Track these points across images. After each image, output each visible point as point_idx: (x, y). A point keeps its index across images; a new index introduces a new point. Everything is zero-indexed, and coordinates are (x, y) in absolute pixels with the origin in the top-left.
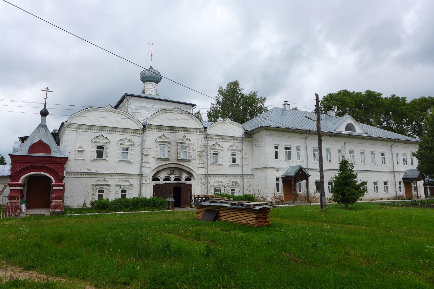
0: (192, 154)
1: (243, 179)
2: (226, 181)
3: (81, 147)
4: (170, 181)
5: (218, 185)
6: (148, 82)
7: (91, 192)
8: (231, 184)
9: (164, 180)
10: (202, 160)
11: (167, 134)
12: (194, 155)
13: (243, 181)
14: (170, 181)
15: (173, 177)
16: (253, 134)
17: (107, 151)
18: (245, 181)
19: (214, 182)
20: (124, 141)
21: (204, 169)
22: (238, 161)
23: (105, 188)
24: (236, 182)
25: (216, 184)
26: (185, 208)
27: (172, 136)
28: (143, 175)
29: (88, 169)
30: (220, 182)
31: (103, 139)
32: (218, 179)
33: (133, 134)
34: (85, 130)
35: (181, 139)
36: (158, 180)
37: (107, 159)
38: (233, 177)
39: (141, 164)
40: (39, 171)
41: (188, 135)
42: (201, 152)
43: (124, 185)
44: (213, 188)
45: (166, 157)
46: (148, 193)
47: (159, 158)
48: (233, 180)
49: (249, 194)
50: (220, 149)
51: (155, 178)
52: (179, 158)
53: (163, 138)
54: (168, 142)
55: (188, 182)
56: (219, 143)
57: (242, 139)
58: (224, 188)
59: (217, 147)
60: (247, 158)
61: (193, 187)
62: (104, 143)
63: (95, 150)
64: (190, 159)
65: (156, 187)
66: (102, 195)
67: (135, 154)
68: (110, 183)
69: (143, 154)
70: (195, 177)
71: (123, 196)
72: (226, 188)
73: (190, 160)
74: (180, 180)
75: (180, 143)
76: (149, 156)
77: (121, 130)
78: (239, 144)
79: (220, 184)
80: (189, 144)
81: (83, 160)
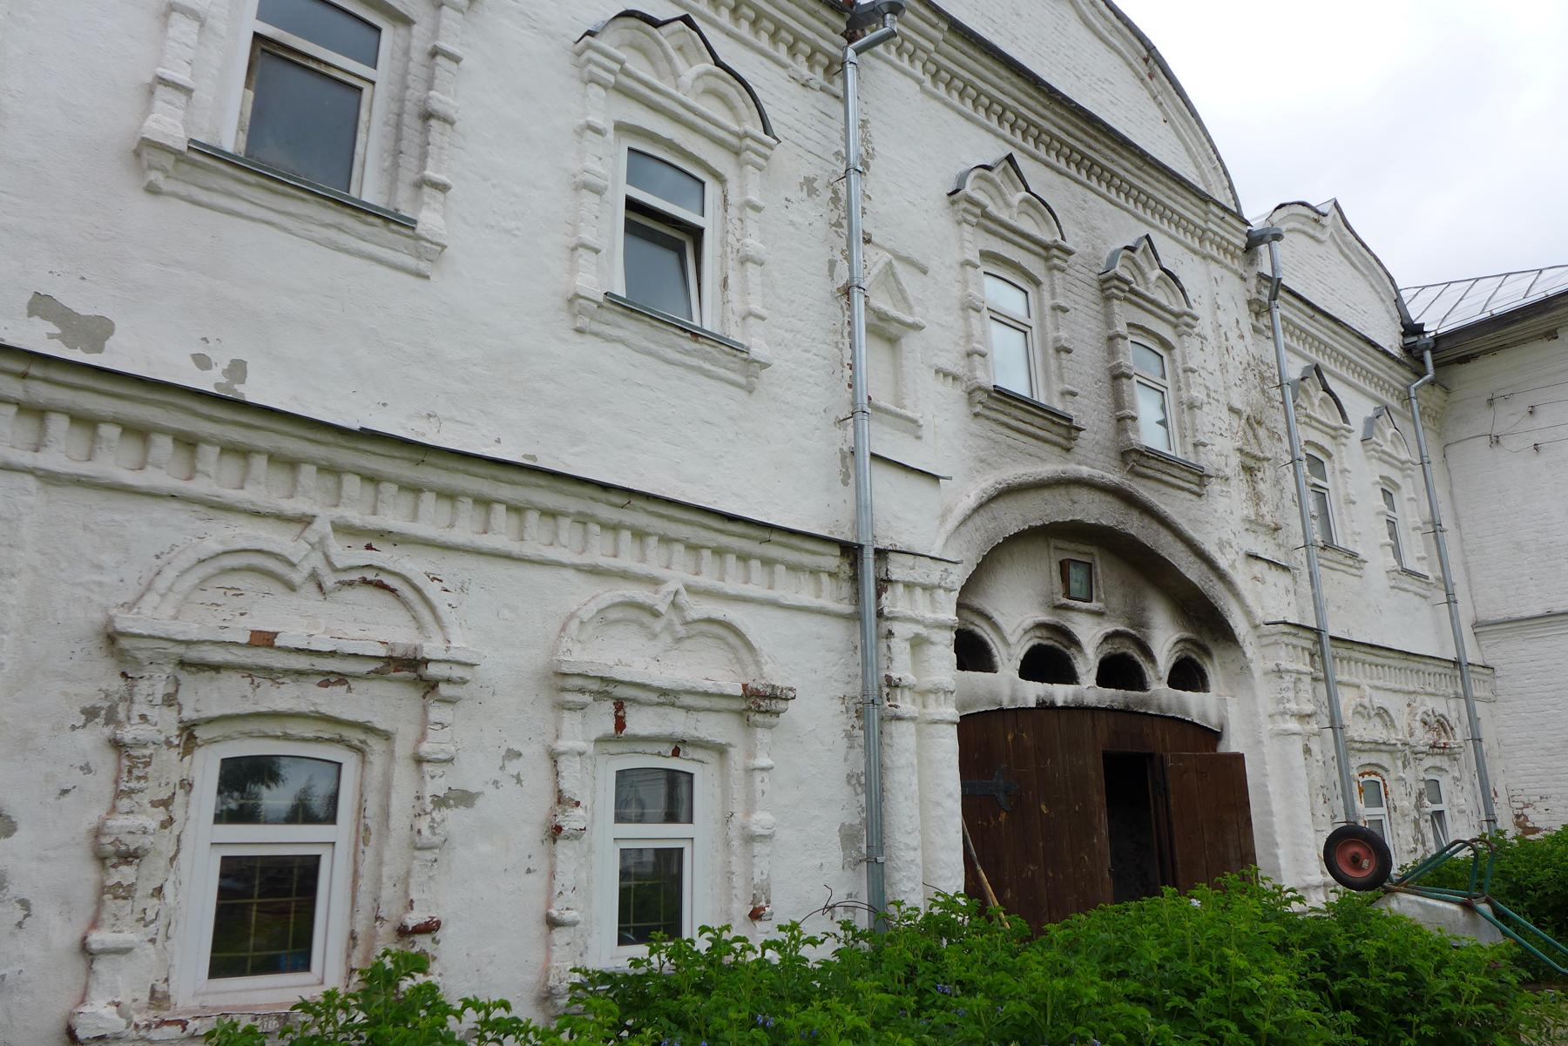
16: (1465, 359)
24: (1442, 725)
28: (898, 569)
30: (1382, 713)
37: (430, 219)
43: (667, 697)
66: (669, 862)
68: (462, 643)
70: (1250, 650)
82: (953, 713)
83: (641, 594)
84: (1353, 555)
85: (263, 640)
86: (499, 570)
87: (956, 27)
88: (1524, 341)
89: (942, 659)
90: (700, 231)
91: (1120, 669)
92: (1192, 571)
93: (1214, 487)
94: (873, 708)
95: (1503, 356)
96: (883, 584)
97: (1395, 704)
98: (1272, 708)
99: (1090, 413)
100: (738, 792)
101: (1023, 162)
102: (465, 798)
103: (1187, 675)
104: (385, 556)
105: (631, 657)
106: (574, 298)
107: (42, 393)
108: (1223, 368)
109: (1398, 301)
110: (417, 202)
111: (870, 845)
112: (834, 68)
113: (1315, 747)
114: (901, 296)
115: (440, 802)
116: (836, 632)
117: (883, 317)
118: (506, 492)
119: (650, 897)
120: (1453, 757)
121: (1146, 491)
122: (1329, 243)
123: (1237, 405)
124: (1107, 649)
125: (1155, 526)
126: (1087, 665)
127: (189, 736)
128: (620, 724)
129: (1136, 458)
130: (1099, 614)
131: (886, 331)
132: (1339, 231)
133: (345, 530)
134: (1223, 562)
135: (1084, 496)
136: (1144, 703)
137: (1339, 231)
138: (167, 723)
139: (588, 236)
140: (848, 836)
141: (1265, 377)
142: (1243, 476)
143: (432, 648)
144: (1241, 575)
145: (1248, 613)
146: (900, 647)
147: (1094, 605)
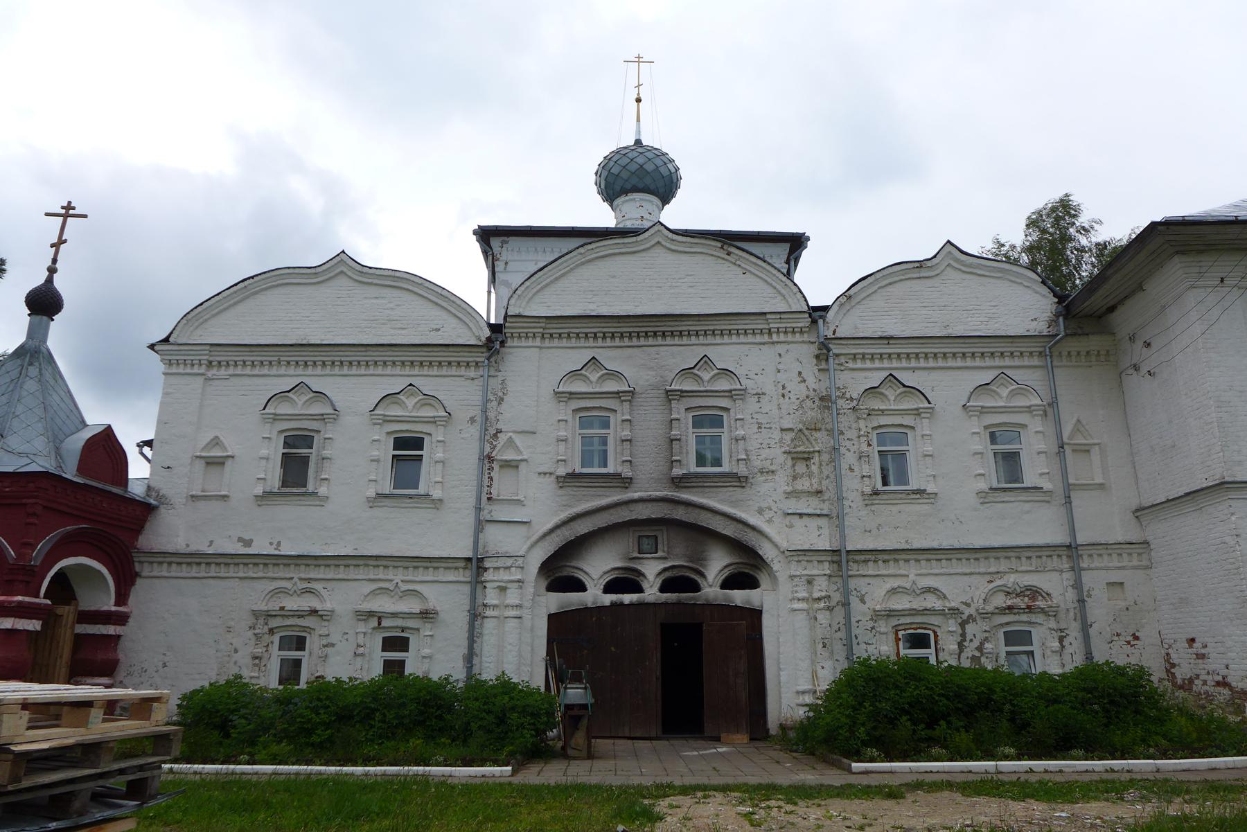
0: (753, 445)
1: (1076, 570)
2: (963, 588)
3: (216, 442)
4: (641, 590)
5: (914, 612)
6: (623, 198)
7: (246, 648)
8: (1000, 601)
9: (609, 588)
10: (810, 475)
11: (612, 358)
12: (765, 453)
13: (1078, 585)
14: (641, 590)
15: (652, 570)
16: (1112, 309)
17: (326, 453)
18: (1094, 581)
19: (894, 591)
20: (401, 404)
21: (823, 522)
22: (1034, 471)
23: (310, 630)
24: (1034, 593)
25: (901, 603)
26: (718, 739)
27: (636, 366)
28: (487, 564)
29: (240, 540)
30: (929, 590)
31: (309, 402)
32: (914, 574)
33: (444, 371)
35: (687, 372)
36: (580, 587)
37: (323, 490)
38: (1014, 563)
39: (479, 509)
41: (725, 354)
42: (802, 433)
43: (394, 615)
44: (883, 626)
45: (610, 469)
46: (516, 651)
47: (573, 477)
48: (1010, 580)
49: (1121, 661)
50: (917, 412)
51: (559, 573)
52: (677, 471)
53: (594, 377)
54: (617, 395)
55: (739, 597)
57: (1046, 347)
58: (953, 626)
59: (892, 399)
60: (1095, 451)
61: (768, 623)
62: (312, 417)
63: (276, 450)
64: (742, 470)
65: (562, 628)
66: (297, 663)
67: (450, 464)
68: (328, 606)
69: (491, 459)
72: (970, 629)
73: (739, 481)
74: (696, 588)
75: (683, 394)
76: (523, 466)
77: (388, 355)
78: (1032, 377)
79: (931, 602)
80: (730, 394)
81: (224, 498)
85: (282, 608)
86: (344, 584)
92: (728, 530)
98: (790, 596)
102: (333, 645)
107: (237, 561)
115: (325, 646)
118: (341, 562)
119: (291, 670)
124: (663, 577)
125: (697, 511)
127: (271, 631)
128: (379, 624)
133: (301, 579)
135: (640, 506)
138: (266, 629)
145: (776, 546)
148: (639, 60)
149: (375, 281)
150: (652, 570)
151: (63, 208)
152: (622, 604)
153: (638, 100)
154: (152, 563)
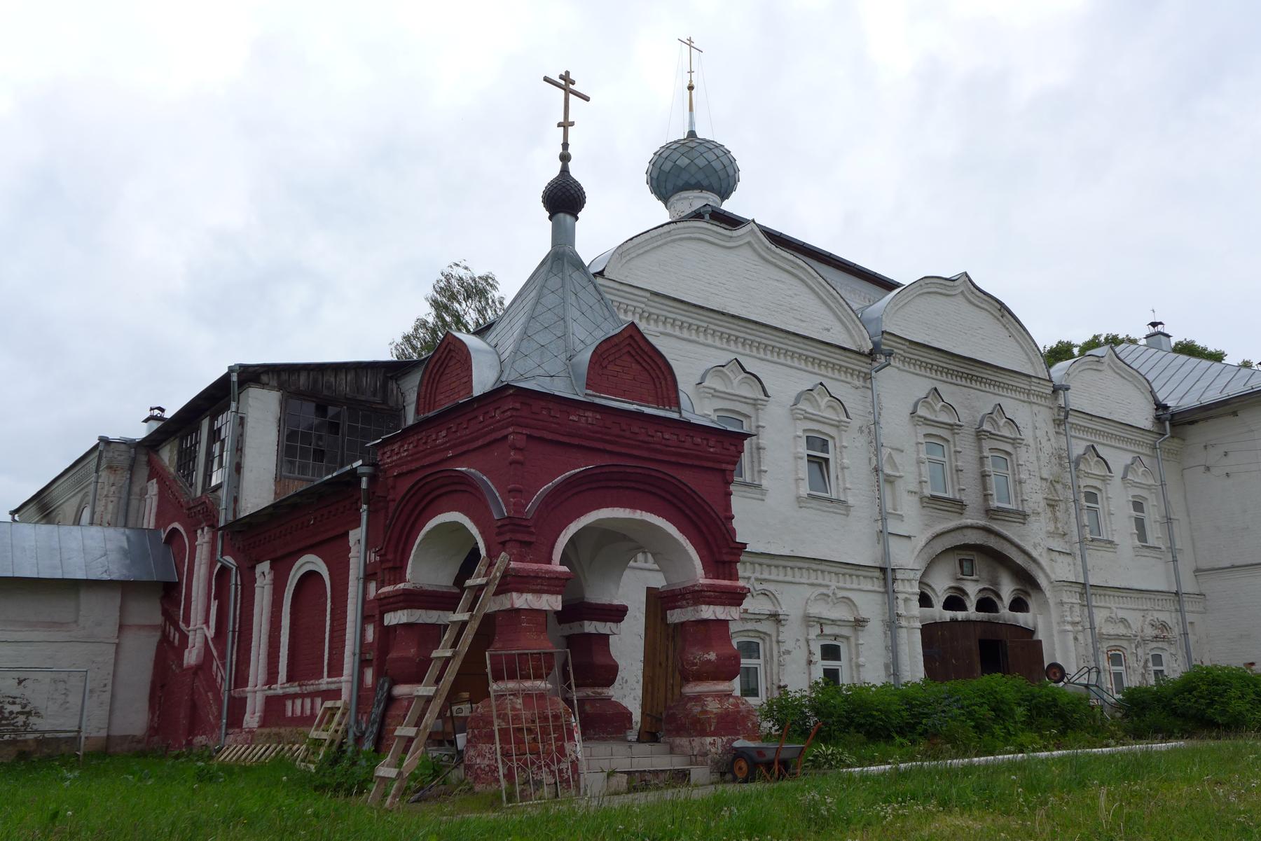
15: (973, 590)
16: (1192, 423)
23: (764, 635)
24: (1164, 626)
28: (899, 575)
30: (1123, 621)
34: (669, 330)
37: (765, 483)
40: (633, 506)
43: (834, 622)
45: (949, 495)
56: (1098, 448)
70: (1048, 594)
71: (832, 675)
82: (919, 625)
83: (824, 591)
84: (1111, 542)
86: (797, 587)
87: (911, 342)
88: (1221, 416)
89: (915, 609)
90: (827, 460)
91: (986, 604)
92: (1020, 560)
93: (1032, 518)
94: (892, 624)
95: (1210, 422)
96: (895, 580)
97: (1130, 616)
99: (972, 497)
100: (854, 651)
101: (940, 387)
102: (788, 652)
103: (1019, 605)
104: (765, 586)
105: (818, 609)
106: (799, 499)
108: (1038, 458)
109: (1152, 392)
110: (760, 479)
111: (893, 666)
112: (867, 377)
113: (1080, 637)
114: (894, 466)
116: (878, 598)
117: (889, 476)
120: (1169, 642)
121: (996, 526)
122: (1110, 372)
123: (1045, 476)
124: (981, 595)
126: (971, 603)
129: (990, 513)
130: (976, 581)
131: (890, 480)
132: (1113, 361)
134: (1035, 554)
135: (969, 532)
136: (997, 618)
137: (1113, 361)
139: (801, 476)
140: (887, 667)
141: (1061, 457)
142: (1048, 510)
143: (780, 612)
144: (1044, 561)
145: (1047, 576)
146: (900, 602)
147: (974, 577)
148: (690, 43)
149: (779, 263)
150: (973, 590)
151: (561, 77)
152: (957, 621)
153: (691, 88)
154: (785, 567)
